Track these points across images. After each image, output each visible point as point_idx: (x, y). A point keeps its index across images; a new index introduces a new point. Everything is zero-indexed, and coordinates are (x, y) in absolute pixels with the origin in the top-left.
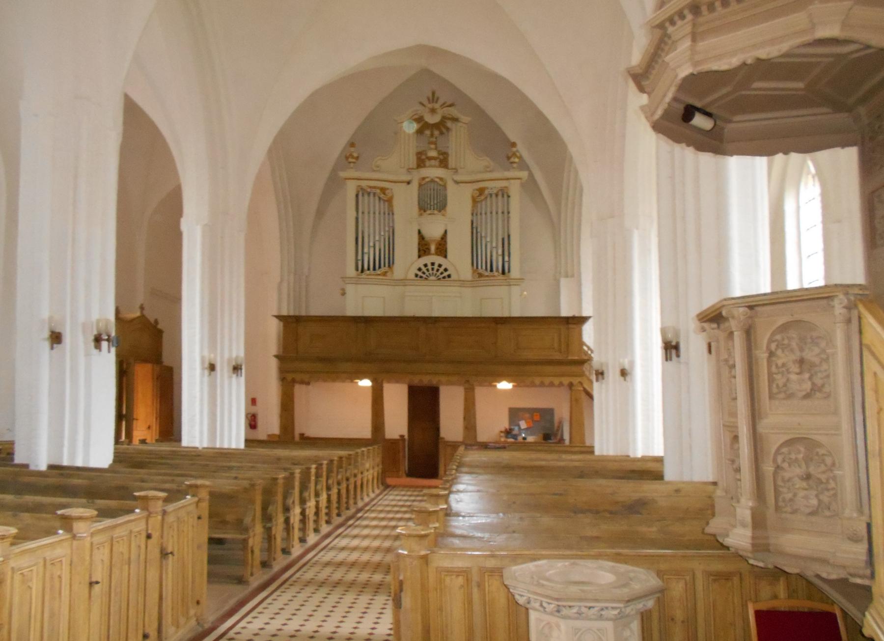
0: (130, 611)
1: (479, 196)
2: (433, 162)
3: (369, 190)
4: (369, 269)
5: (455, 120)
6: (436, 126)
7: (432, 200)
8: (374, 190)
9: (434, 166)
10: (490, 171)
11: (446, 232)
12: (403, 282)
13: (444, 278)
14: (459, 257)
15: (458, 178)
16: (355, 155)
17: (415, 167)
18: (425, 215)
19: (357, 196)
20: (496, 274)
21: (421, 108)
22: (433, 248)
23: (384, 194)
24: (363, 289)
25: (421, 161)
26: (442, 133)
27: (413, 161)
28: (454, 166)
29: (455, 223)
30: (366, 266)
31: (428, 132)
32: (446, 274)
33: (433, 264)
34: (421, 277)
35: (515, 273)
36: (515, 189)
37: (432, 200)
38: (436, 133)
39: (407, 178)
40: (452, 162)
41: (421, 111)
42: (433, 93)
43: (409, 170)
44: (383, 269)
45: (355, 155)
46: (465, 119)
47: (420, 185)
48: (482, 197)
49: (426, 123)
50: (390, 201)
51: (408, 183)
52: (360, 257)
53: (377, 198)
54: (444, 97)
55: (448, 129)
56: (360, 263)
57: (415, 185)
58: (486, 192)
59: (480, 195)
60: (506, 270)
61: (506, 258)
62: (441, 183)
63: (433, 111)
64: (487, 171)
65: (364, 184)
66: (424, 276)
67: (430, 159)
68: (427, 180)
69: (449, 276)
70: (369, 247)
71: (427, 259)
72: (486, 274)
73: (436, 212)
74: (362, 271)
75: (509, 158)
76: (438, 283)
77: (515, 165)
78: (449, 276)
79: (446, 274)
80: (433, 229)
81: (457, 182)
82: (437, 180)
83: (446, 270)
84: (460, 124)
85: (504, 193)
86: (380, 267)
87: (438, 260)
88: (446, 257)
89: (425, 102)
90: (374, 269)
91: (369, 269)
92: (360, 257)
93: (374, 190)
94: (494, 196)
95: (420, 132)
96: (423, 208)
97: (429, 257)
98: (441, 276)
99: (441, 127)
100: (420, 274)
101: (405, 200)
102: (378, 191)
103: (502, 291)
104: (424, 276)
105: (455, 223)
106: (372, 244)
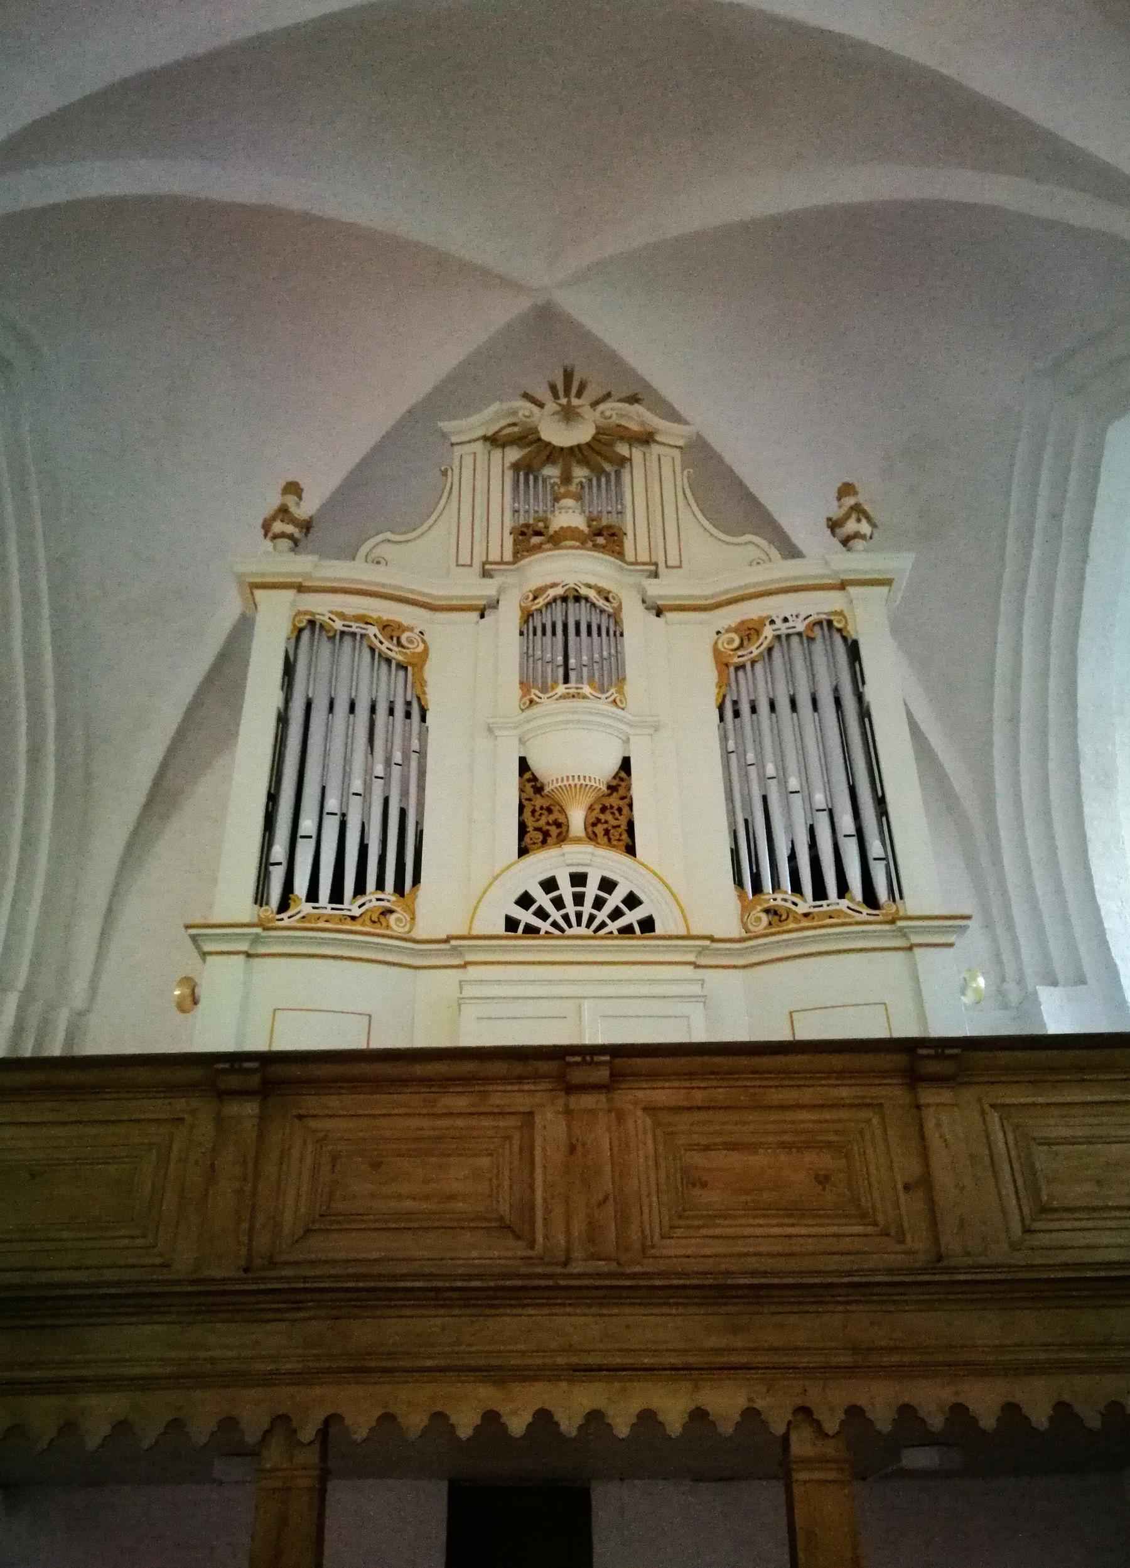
5: (646, 439)
6: (577, 454)
7: (570, 642)
11: (626, 765)
13: (627, 930)
17: (508, 556)
18: (547, 705)
22: (577, 819)
25: (530, 537)
27: (501, 545)
28: (644, 557)
30: (301, 886)
31: (552, 472)
32: (632, 917)
34: (531, 930)
37: (570, 642)
38: (580, 473)
39: (487, 589)
40: (636, 545)
42: (568, 375)
48: (754, 650)
52: (279, 852)
55: (623, 462)
57: (509, 617)
58: (768, 632)
60: (882, 894)
61: (875, 849)
62: (601, 603)
63: (569, 415)
65: (321, 606)
68: (552, 593)
69: (647, 925)
71: (555, 861)
73: (587, 690)
78: (647, 925)
79: (632, 917)
80: (577, 748)
82: (592, 594)
83: (632, 901)
84: (655, 449)
86: (360, 889)
87: (599, 861)
88: (631, 850)
90: (337, 896)
92: (279, 852)
95: (525, 470)
98: (613, 926)
100: (526, 917)
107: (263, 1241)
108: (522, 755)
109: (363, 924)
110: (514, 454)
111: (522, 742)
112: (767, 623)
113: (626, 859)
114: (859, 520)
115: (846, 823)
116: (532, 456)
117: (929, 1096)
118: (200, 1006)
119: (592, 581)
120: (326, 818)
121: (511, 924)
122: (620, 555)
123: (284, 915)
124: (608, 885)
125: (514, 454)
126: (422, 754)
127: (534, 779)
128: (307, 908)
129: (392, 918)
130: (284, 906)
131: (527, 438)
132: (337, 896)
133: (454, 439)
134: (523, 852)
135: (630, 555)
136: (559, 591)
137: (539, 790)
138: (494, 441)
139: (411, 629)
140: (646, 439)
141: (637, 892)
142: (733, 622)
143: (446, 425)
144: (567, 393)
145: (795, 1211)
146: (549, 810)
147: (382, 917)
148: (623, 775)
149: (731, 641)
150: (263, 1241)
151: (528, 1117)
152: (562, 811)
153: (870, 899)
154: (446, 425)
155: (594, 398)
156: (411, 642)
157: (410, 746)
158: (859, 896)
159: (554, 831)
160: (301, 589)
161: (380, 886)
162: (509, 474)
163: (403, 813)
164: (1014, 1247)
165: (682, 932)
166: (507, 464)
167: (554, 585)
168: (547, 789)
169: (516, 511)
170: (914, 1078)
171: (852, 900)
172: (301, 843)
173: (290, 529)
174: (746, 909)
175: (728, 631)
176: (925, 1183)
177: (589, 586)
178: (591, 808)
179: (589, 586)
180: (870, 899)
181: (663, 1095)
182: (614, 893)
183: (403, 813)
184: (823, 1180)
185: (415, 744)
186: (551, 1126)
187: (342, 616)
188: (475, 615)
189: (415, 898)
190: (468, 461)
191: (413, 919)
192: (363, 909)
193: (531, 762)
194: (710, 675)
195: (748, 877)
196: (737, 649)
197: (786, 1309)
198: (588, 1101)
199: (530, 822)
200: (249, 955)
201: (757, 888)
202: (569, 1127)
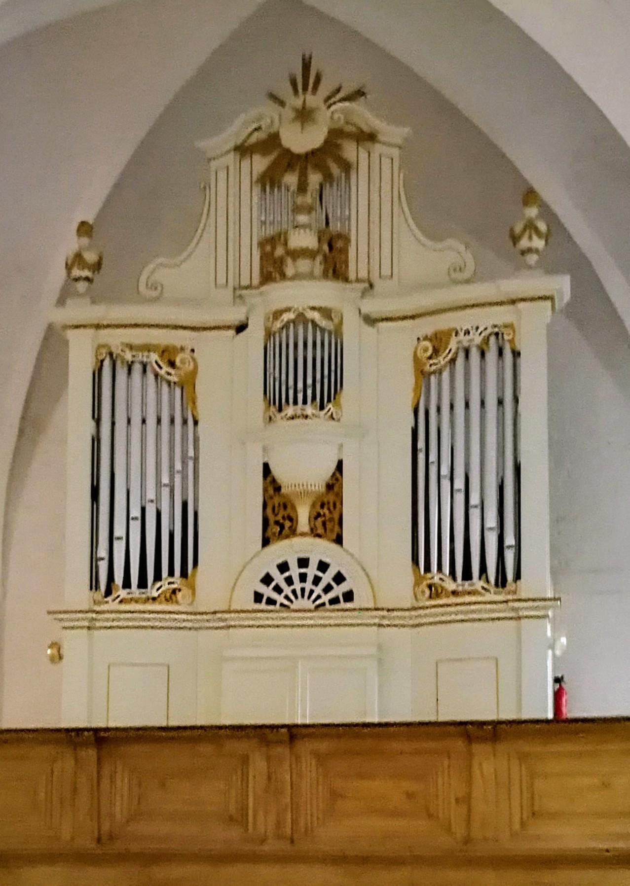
0: (378, 185)
1: (436, 356)
2: (304, 265)
3: (128, 356)
4: (127, 584)
5: (368, 137)
6: (313, 159)
7: (305, 376)
8: (141, 356)
9: (311, 276)
10: (468, 281)
11: (340, 465)
12: (222, 618)
13: (335, 601)
14: (375, 544)
15: (371, 306)
16: (90, 257)
17: (256, 281)
18: (280, 422)
19: (97, 375)
20: (478, 583)
21: (270, 111)
23: (172, 364)
24: (113, 644)
25: (272, 268)
26: (328, 177)
27: (250, 264)
28: (363, 274)
29: (363, 441)
31: (291, 179)
33: (303, 563)
34: (271, 602)
35: (537, 578)
36: (533, 329)
37: (305, 376)
38: (315, 179)
39: (235, 316)
40: (357, 265)
41: (270, 116)
42: (306, 66)
43: (239, 292)
44: (165, 585)
45: (90, 257)
46: (394, 133)
47: (269, 334)
48: (442, 360)
49: (288, 151)
50: (187, 386)
51: (241, 328)
53: (151, 376)
54: (335, 72)
55: (347, 167)
56: (103, 566)
57: (255, 334)
58: (453, 345)
59: (436, 352)
60: (510, 576)
61: (510, 540)
62: (323, 323)
63: (304, 116)
64: (456, 282)
65: (115, 339)
66: (280, 599)
67: (296, 254)
68: (287, 317)
69: (349, 596)
70: (159, 484)
71: (287, 550)
72: (450, 586)
73: (309, 410)
74: (108, 592)
75: (515, 239)
76: (318, 617)
77: (532, 259)
78: (349, 596)
79: (338, 591)
81: (370, 320)
82: (316, 316)
83: (339, 578)
84: (378, 148)
85: (502, 346)
86: (158, 577)
87: (319, 549)
88: (339, 540)
89: (285, 92)
90: (143, 584)
91: (127, 584)
92: (103, 552)
93: (141, 356)
94: (475, 355)
95: (269, 180)
96: (276, 400)
97: (296, 541)
98: (325, 598)
99: (328, 160)
100: (268, 592)
101: (231, 374)
102: (154, 357)
103: (492, 636)
104: (280, 599)
105: (363, 441)
106: (135, 512)
107: (106, 827)
108: (266, 460)
109: (160, 603)
110: (260, 163)
111: (265, 450)
112: (454, 334)
113: (335, 546)
114: (530, 238)
115: (475, 515)
116: (279, 164)
117: (477, 748)
118: (64, 660)
119: (317, 304)
120: (131, 522)
121: (258, 597)
122: (346, 280)
123: (109, 599)
124: (323, 567)
125: (260, 163)
126: (196, 459)
127: (274, 481)
128: (123, 593)
129: (179, 595)
130: (108, 592)
131: (272, 141)
132: (143, 584)
133: (209, 155)
134: (266, 542)
135: (352, 276)
136: (291, 316)
137: (278, 489)
138: (243, 150)
139: (182, 349)
140: (371, 137)
141: (343, 572)
142: (429, 331)
143: (202, 144)
144: (305, 89)
145: (395, 814)
146: (285, 507)
147: (173, 596)
148: (338, 475)
149: (426, 350)
150: (106, 827)
151: (245, 760)
152: (294, 508)
153: (501, 581)
154: (202, 144)
155: (327, 93)
156: (183, 361)
157: (187, 454)
158: (492, 579)
159: (287, 524)
160: (98, 327)
161: (171, 573)
162: (257, 190)
163: (185, 505)
164: (514, 835)
165: (371, 606)
166: (254, 179)
167: (288, 310)
168: (283, 490)
169: (264, 223)
170: (469, 739)
171: (488, 581)
172: (116, 544)
173: (86, 273)
174: (417, 584)
175: (426, 338)
176: (466, 800)
177: (313, 308)
178: (313, 506)
179: (313, 308)
180: (501, 581)
181: (323, 746)
182: (327, 573)
183: (185, 505)
184: (410, 795)
185: (191, 453)
186: (258, 765)
187: (131, 347)
188: (232, 332)
189: (194, 575)
190: (222, 175)
191: (194, 594)
192: (160, 591)
193: (271, 466)
194: (409, 379)
195: (420, 556)
196: (430, 358)
197: (525, 802)
198: (280, 750)
199: (272, 518)
200: (89, 628)
201: (428, 569)
202: (269, 768)
